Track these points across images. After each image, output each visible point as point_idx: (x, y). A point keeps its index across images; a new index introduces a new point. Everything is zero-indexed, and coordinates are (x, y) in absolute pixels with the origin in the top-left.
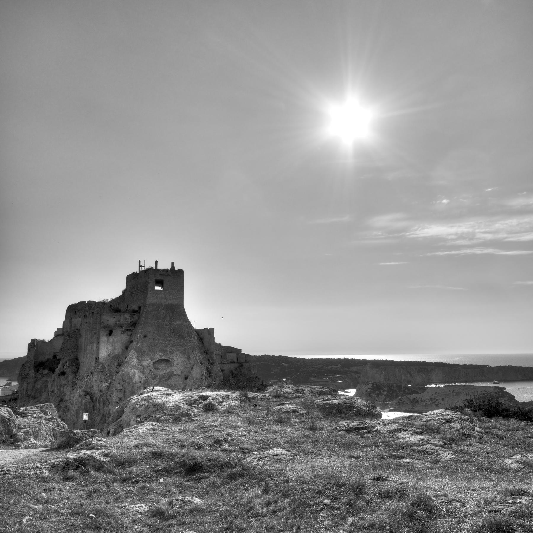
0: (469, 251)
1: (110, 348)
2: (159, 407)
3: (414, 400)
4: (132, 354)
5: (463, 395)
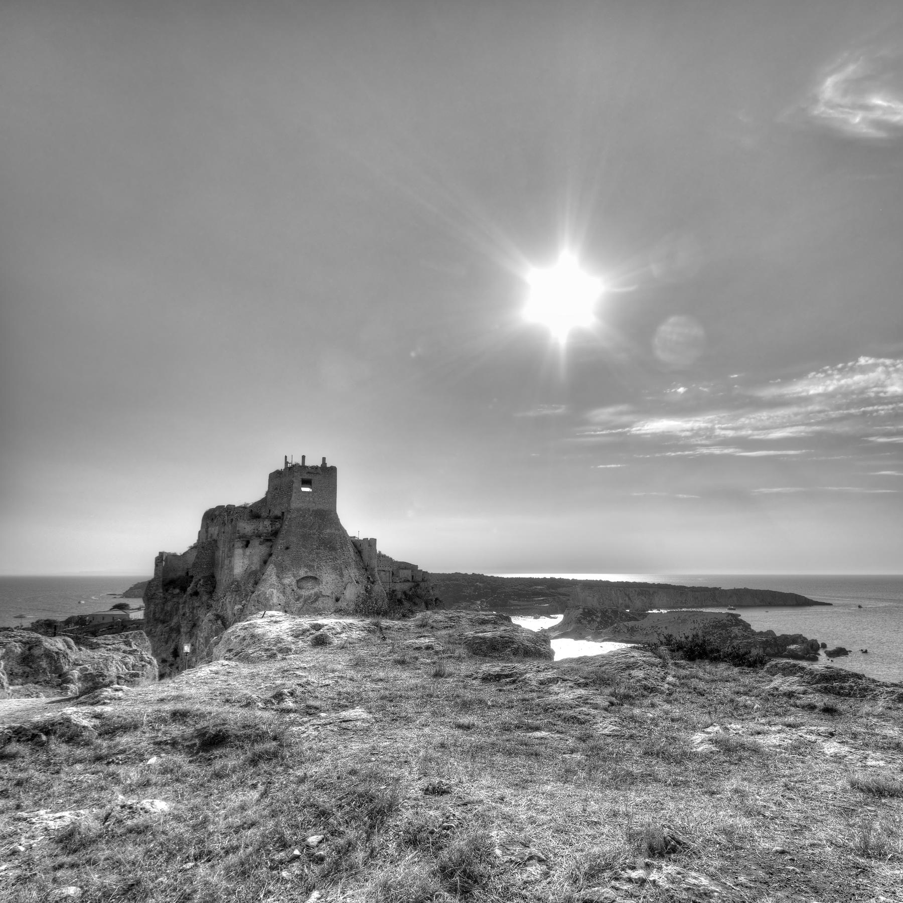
0: (705, 451)
1: (246, 562)
2: (256, 639)
3: (632, 628)
4: (271, 570)
5: (690, 623)
